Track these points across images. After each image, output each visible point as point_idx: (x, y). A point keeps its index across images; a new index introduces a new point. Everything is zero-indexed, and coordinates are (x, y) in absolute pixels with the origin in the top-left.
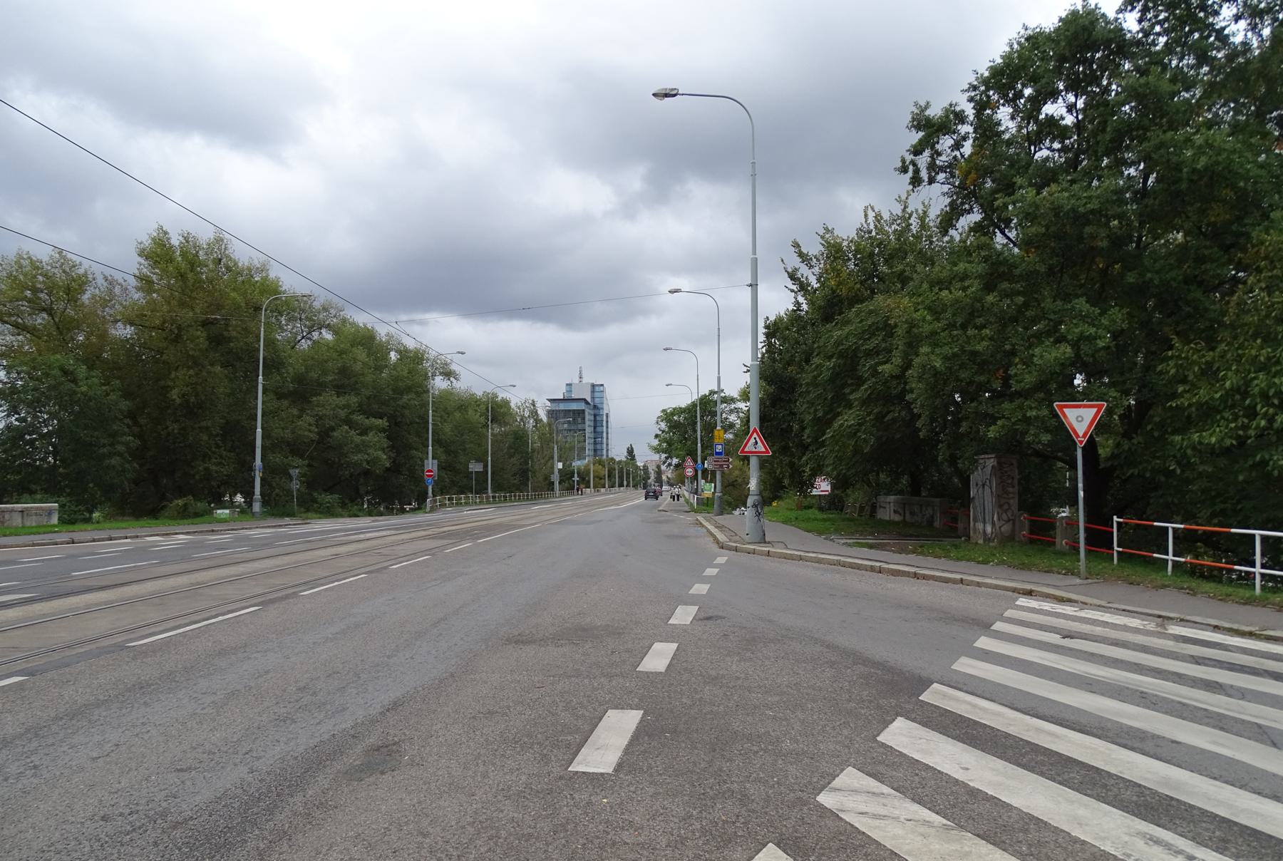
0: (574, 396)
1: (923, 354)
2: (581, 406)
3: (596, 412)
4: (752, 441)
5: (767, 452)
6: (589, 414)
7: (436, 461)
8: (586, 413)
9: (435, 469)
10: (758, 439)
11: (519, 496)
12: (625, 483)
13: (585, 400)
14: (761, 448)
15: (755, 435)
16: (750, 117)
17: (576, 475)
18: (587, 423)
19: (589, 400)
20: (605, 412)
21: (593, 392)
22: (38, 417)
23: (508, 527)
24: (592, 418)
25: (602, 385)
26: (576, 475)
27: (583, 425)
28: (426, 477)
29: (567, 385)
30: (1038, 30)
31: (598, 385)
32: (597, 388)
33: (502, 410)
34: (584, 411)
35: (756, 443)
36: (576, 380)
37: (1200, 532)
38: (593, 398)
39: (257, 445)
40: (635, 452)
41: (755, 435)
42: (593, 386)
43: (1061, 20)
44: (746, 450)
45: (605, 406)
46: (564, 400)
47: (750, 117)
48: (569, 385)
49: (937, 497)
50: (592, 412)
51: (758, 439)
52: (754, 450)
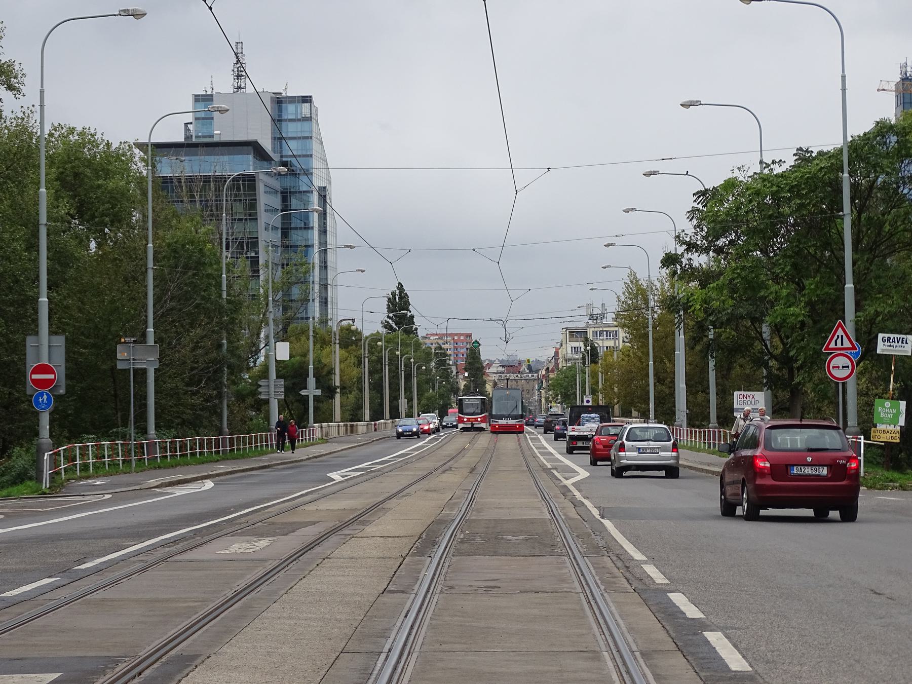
0: (221, 132)
1: (692, 319)
2: (245, 165)
3: (289, 182)
6: (271, 191)
7: (60, 341)
8: (261, 188)
9: (59, 362)
11: (183, 447)
12: (403, 404)
17: (311, 381)
18: (264, 218)
19: (267, 145)
20: (318, 182)
21: (278, 121)
22: (825, 222)
24: (276, 202)
25: (307, 99)
26: (311, 381)
27: (250, 226)
28: (30, 387)
29: (197, 98)
31: (293, 100)
32: (290, 111)
33: (111, 185)
36: (224, 85)
38: (279, 139)
40: (416, 308)
42: (279, 101)
43: (803, 156)
45: (316, 164)
46: (188, 147)
48: (203, 99)
50: (276, 184)
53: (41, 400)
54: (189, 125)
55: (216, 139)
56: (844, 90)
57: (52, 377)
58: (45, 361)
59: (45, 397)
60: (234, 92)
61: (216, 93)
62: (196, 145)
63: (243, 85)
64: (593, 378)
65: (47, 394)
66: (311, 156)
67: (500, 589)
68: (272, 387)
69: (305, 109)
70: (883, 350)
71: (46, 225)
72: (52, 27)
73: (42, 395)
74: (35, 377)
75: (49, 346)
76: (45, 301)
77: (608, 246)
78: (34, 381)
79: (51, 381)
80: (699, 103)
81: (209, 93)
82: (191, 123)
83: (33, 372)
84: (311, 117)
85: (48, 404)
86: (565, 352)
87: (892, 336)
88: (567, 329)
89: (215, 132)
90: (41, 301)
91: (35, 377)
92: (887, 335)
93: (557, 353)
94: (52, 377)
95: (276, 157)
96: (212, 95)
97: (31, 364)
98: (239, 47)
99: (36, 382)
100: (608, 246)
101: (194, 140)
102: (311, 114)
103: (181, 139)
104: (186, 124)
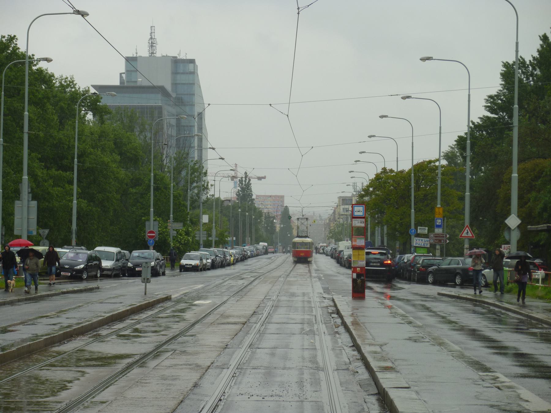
0: (141, 81)
2: (155, 100)
4: (466, 231)
5: (473, 237)
10: (468, 230)
13: (162, 90)
14: (470, 235)
15: (467, 229)
16: (459, 62)
19: (169, 87)
20: (197, 110)
21: (175, 73)
23: (53, 331)
30: (468, 367)
34: (160, 108)
35: (468, 232)
37: (80, 190)
38: (175, 85)
39: (73, 214)
41: (467, 229)
42: (176, 61)
44: (463, 235)
45: (196, 99)
47: (459, 62)
49: (387, 244)
51: (468, 230)
52: (467, 236)
53: (150, 242)
54: (122, 75)
55: (138, 84)
56: (469, 101)
57: (154, 235)
58: (152, 230)
59: (152, 241)
60: (150, 56)
61: (139, 56)
62: (127, 87)
63: (155, 52)
64: (38, 398)
65: (152, 240)
66: (194, 94)
67: (281, 398)
68: (201, 234)
69: (191, 66)
70: (419, 232)
71: (28, 133)
72: (42, 14)
73: (151, 240)
74: (149, 235)
75: (28, 207)
76: (26, 178)
77: (352, 177)
78: (148, 236)
79: (153, 236)
80: (431, 59)
81: (135, 56)
82: (124, 73)
83: (148, 233)
84: (194, 72)
85: (153, 244)
86: (339, 211)
87: (422, 227)
88: (340, 197)
89: (139, 80)
90: (24, 178)
91: (149, 235)
92: (420, 227)
93: (334, 212)
94: (154, 235)
95: (174, 95)
96: (136, 57)
97: (147, 230)
98: (152, 29)
99: (150, 236)
100: (352, 177)
101: (126, 84)
102: (194, 70)
103: (117, 83)
104: (121, 74)
